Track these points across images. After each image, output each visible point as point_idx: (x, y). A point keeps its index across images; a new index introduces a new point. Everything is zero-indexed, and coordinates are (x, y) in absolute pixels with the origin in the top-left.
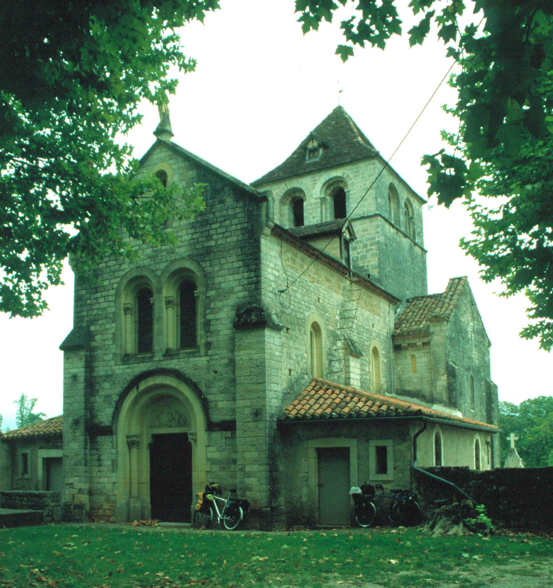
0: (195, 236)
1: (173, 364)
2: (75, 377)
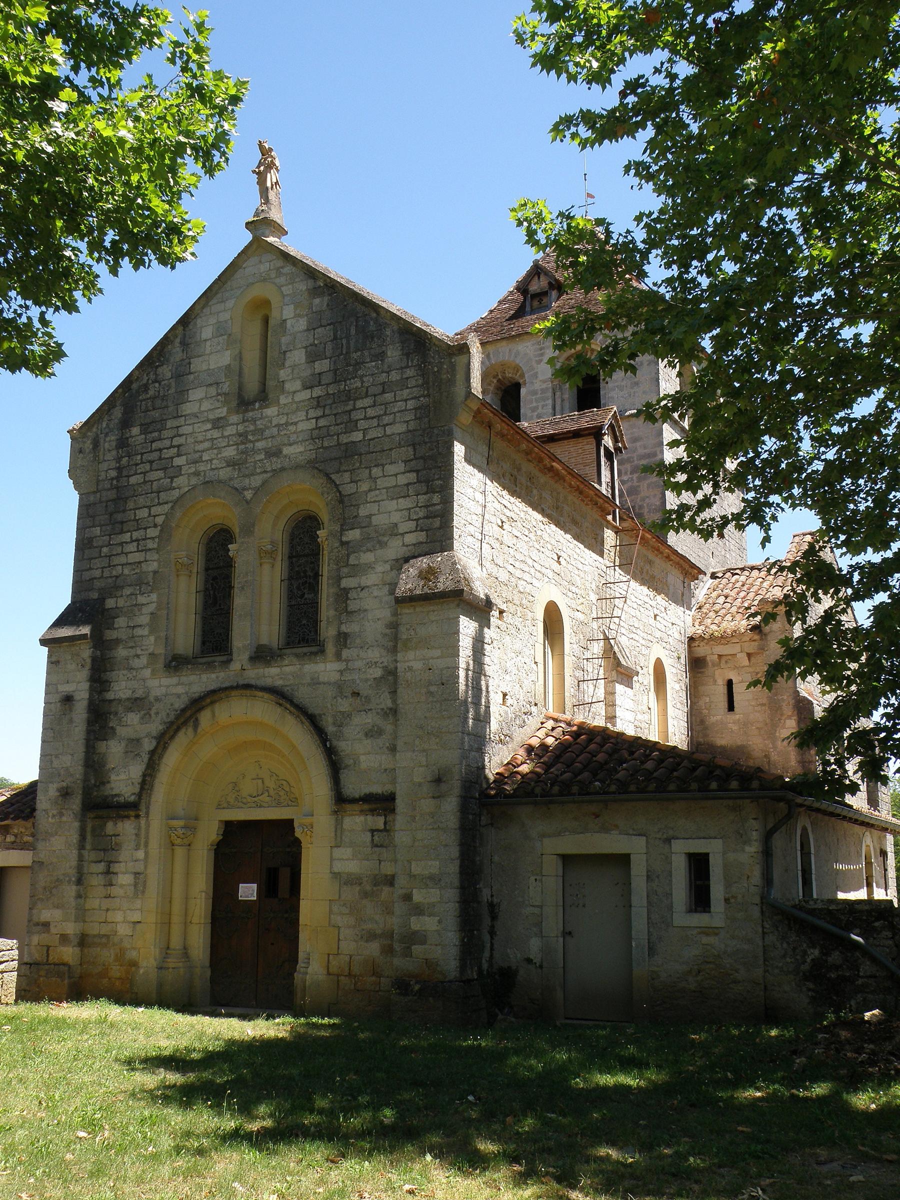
0: (322, 422)
1: (272, 674)
2: (68, 699)
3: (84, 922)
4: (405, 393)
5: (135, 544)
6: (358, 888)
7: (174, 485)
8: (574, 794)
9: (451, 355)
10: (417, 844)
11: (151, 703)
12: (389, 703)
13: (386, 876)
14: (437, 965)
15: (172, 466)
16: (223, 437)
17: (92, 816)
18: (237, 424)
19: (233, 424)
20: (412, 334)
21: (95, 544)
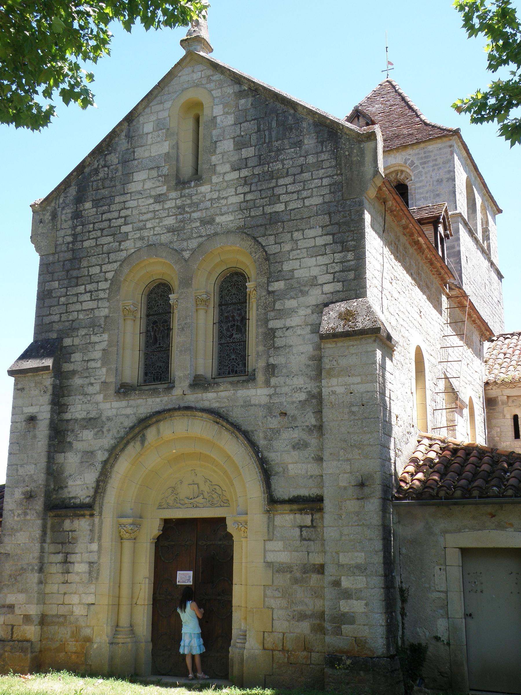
0: (249, 197)
1: (209, 398)
2: (32, 419)
3: (44, 604)
4: (321, 172)
5: (89, 294)
6: (289, 576)
7: (121, 247)
8: (475, 498)
9: (360, 142)
10: (343, 538)
11: (103, 422)
12: (313, 422)
13: (314, 565)
14: (366, 643)
15: (120, 233)
16: (164, 209)
17: (52, 515)
18: (176, 199)
19: (172, 199)
20: (327, 126)
21: (54, 295)
